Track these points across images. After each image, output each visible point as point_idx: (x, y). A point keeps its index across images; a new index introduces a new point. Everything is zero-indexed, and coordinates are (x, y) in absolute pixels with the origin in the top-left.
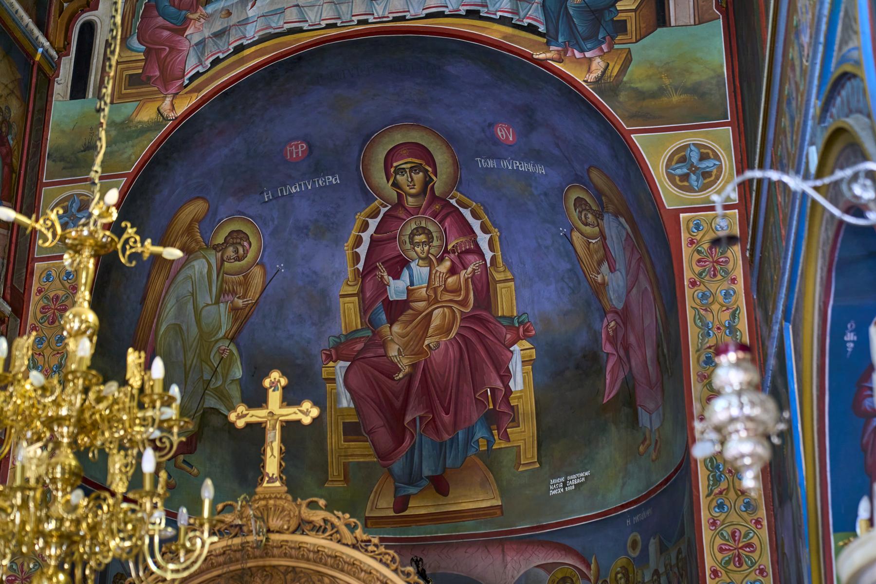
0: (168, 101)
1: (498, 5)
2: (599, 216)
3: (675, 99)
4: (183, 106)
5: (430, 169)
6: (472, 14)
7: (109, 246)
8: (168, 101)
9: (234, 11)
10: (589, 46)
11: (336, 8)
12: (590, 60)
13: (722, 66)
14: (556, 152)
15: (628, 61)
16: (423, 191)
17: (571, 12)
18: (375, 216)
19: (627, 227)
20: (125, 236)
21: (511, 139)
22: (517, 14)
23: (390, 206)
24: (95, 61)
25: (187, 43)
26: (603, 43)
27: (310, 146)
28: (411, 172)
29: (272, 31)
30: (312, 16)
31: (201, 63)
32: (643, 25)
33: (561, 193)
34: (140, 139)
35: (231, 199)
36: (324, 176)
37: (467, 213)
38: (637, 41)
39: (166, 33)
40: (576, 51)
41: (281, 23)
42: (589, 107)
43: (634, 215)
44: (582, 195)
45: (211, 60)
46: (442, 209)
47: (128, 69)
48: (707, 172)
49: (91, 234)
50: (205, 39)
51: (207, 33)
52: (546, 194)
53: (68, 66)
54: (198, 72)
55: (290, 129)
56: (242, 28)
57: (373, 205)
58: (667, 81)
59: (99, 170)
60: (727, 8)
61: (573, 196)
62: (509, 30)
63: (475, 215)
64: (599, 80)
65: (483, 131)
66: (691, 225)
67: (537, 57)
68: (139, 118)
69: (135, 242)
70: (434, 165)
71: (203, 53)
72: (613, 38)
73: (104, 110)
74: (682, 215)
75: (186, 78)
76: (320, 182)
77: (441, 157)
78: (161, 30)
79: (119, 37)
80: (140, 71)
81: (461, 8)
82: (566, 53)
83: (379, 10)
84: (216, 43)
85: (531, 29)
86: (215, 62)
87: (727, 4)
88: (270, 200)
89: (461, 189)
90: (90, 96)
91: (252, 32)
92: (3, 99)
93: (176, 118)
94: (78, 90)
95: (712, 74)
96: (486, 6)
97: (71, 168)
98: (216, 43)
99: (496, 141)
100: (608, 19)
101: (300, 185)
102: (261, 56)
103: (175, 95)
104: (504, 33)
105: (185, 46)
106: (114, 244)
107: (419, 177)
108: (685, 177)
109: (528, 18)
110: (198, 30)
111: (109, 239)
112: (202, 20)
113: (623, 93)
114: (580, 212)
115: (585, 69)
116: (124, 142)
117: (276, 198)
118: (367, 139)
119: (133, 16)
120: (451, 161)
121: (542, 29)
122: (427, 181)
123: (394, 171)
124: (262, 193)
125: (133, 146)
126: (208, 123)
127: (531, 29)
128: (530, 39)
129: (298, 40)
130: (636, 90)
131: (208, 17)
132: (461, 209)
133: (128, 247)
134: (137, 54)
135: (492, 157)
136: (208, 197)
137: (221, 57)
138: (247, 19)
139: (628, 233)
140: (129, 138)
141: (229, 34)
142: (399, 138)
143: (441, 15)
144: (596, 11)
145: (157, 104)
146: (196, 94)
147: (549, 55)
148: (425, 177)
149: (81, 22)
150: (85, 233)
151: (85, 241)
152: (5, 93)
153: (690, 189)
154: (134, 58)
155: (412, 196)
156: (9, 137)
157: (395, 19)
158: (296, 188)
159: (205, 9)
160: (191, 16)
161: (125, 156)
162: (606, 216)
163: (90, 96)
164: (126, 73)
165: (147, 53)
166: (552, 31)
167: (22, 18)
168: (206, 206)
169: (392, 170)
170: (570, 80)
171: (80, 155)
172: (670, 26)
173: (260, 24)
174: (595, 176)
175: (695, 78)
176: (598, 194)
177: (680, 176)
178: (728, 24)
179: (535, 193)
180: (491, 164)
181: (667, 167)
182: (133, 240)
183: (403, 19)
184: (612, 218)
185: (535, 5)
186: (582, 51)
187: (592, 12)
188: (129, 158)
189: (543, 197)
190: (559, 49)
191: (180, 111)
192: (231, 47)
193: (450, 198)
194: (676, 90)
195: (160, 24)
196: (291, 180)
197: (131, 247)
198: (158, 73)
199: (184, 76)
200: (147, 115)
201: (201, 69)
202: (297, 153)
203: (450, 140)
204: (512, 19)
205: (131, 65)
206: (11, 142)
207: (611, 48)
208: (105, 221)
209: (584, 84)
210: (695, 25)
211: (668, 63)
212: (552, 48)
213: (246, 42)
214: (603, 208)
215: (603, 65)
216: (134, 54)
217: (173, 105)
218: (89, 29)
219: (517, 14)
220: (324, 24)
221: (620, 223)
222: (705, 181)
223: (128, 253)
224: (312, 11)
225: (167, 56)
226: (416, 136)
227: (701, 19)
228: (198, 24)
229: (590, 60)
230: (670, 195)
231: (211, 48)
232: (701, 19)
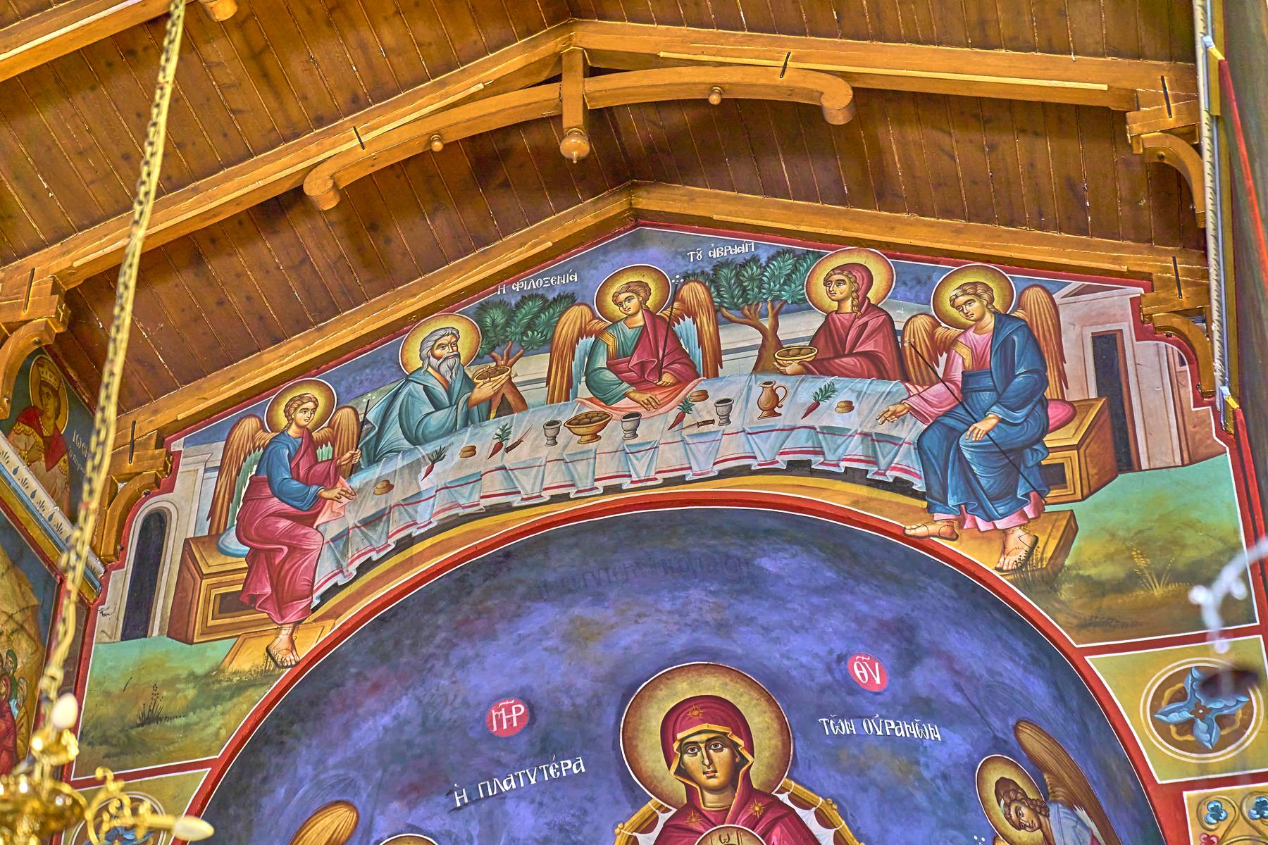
0: (285, 633)
1: (841, 450)
2: (1040, 809)
3: (1158, 591)
4: (309, 642)
5: (741, 742)
6: (797, 467)
7: (68, 813)
8: (285, 633)
9: (397, 482)
10: (1001, 510)
11: (568, 468)
12: (1005, 532)
13: (1236, 532)
14: (957, 699)
15: (1071, 531)
16: (731, 782)
17: (968, 456)
18: (647, 826)
19: (1091, 825)
20: (102, 796)
21: (878, 681)
22: (875, 463)
23: (674, 810)
24: (165, 574)
25: (318, 537)
26: (1025, 503)
27: (531, 708)
28: (707, 747)
29: (461, 512)
30: (527, 484)
32: (1093, 471)
33: (972, 772)
34: (235, 700)
35: (396, 805)
36: (557, 761)
37: (808, 817)
38: (1084, 499)
39: (284, 524)
40: (978, 520)
41: (476, 498)
42: (1011, 615)
43: (1103, 804)
44: (1009, 774)
45: (357, 563)
46: (765, 812)
47: (220, 585)
48: (1225, 716)
49: (35, 791)
50: (348, 530)
51: (352, 520)
52: (945, 777)
53: (120, 585)
54: (336, 584)
55: (499, 676)
56: (409, 508)
57: (644, 809)
58: (1142, 563)
59: (59, 675)
60: (1237, 434)
61: (993, 777)
62: (863, 491)
63: (824, 821)
64: (1022, 566)
65: (829, 669)
66: (1205, 811)
67: (912, 532)
68: (235, 666)
69: (121, 807)
70: (743, 728)
71: (344, 554)
72: (1041, 495)
73: (74, 568)
74: (1186, 794)
75: (315, 595)
76: (552, 771)
77: (759, 718)
78: (273, 519)
79: (110, 442)
80: (240, 588)
81: (778, 458)
82: (961, 523)
83: (640, 468)
84: (365, 535)
85: (900, 486)
86: (362, 569)
87: (1236, 428)
88: (464, 805)
89: (795, 775)
90: (156, 633)
91: (426, 515)
92: (4, 638)
93: (298, 663)
94: (136, 625)
95: (1220, 546)
96: (822, 453)
97: (116, 755)
98: (365, 535)
99: (852, 687)
100: (1030, 464)
101: (516, 778)
102: (441, 554)
104: (857, 495)
105: (314, 541)
106: (77, 811)
107: (722, 756)
108: (1187, 727)
109: (894, 469)
110: (337, 516)
111: (69, 802)
112: (343, 499)
113: (1066, 586)
114: (1008, 805)
115: (998, 549)
116: (208, 708)
117: (475, 800)
118: (629, 691)
119: (231, 500)
120: (776, 726)
121: (919, 485)
122: (737, 763)
123: (679, 749)
124: (451, 793)
125: (223, 714)
126: (353, 670)
127: (900, 486)
128: (898, 504)
129: (504, 524)
130: (1088, 580)
131: (352, 494)
132: (798, 810)
133: (106, 817)
134: (235, 559)
135: (849, 714)
136: (356, 803)
137: (374, 559)
138: (419, 493)
139: (1093, 838)
140: (218, 699)
141: (389, 521)
142: (684, 689)
143: (745, 471)
144: (1011, 451)
145: (265, 641)
146: (331, 622)
147: (932, 529)
148: (733, 756)
149: (146, 512)
150: (23, 787)
151: (24, 803)
152: (9, 627)
153: (1198, 748)
154: (229, 567)
155: (713, 790)
156: (13, 703)
157: (668, 483)
158: (509, 782)
159: (349, 481)
160: (326, 494)
161: (210, 730)
162: (1053, 809)
163: (156, 633)
164: (214, 592)
165: (252, 557)
166: (936, 488)
167: (42, 505)
168: (353, 816)
169: (676, 745)
170: (973, 569)
171: (133, 732)
172: (1140, 470)
173: (441, 500)
174: (1029, 738)
175: (1191, 555)
176: (1037, 769)
177: (1176, 725)
178: (1242, 459)
179: (927, 775)
180: (846, 727)
181: (1154, 709)
182: (116, 803)
183: (681, 481)
184: (1063, 810)
185: (905, 446)
186: (990, 518)
187: (1003, 452)
188: (217, 734)
189: (940, 782)
190: (951, 517)
191: (304, 651)
192: (391, 541)
193: (779, 792)
194: (1159, 577)
195: (274, 509)
196: (503, 769)
197: (112, 816)
198: (268, 590)
199: (311, 593)
200: (249, 660)
201: (340, 580)
202: (510, 721)
203: (773, 688)
204: (867, 471)
205: (223, 578)
206: (15, 712)
207: (1039, 510)
208: (55, 760)
209: (996, 573)
210: (1183, 465)
211: (1140, 532)
212: (937, 516)
213: (416, 532)
214: (1046, 795)
215: (1027, 540)
216: (230, 559)
217: (292, 642)
218: (157, 523)
219: (875, 463)
220: (546, 496)
221: (1079, 819)
222: (1224, 733)
223: (105, 827)
224: (527, 475)
225: (284, 561)
226: (713, 685)
228: (336, 506)
229: (1005, 532)
230: (1164, 762)
231: (357, 542)
232: (1193, 457)
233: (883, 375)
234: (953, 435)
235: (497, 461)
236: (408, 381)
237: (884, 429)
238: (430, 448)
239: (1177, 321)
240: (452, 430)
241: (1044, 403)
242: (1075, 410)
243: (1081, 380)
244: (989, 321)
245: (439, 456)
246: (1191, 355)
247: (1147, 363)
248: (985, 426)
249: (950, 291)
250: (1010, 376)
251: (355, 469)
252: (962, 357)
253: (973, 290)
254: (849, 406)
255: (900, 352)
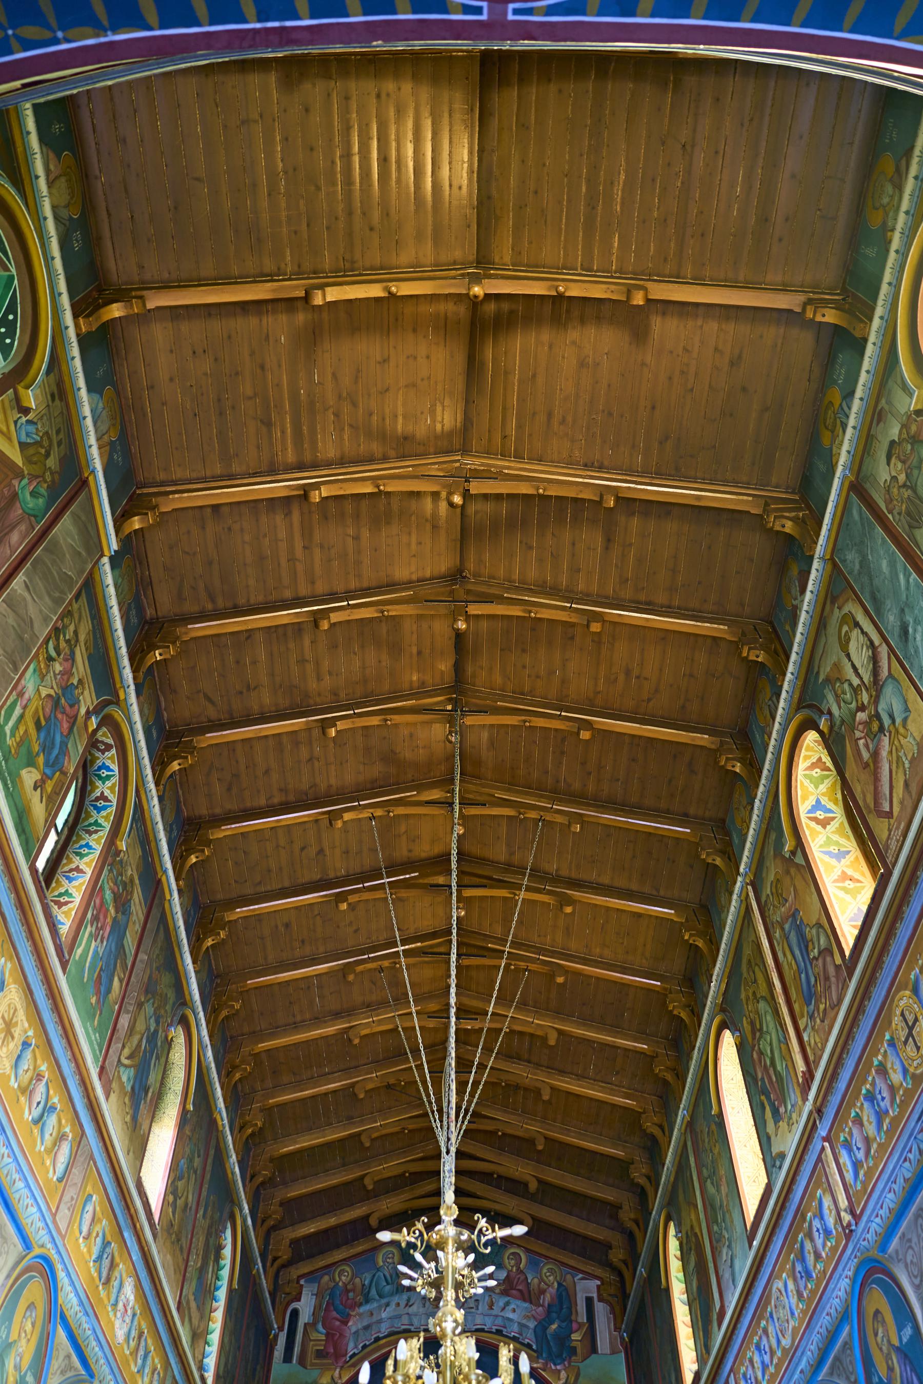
12: (559, 1371)
31: (356, 1347)
39: (338, 1323)
51: (360, 1327)
85: (529, 1346)
94: (287, 1358)
103: (342, 1368)
127: (529, 1346)
131: (360, 1315)
165: (327, 1335)
218: (295, 1314)
227: (614, 1352)
232: (614, 1352)
233: (524, 1300)
234: (545, 1329)
235: (406, 1311)
236: (378, 1270)
237: (524, 1322)
238: (384, 1301)
239: (610, 1298)
240: (392, 1295)
241: (571, 1321)
242: (581, 1325)
243: (583, 1318)
244: (556, 1284)
245: (388, 1305)
246: (613, 1311)
247: (600, 1308)
248: (554, 1326)
249: (545, 1270)
250: (561, 1309)
251: (361, 1305)
252: (548, 1297)
253: (549, 1270)
254: (514, 1311)
255: (529, 1292)
